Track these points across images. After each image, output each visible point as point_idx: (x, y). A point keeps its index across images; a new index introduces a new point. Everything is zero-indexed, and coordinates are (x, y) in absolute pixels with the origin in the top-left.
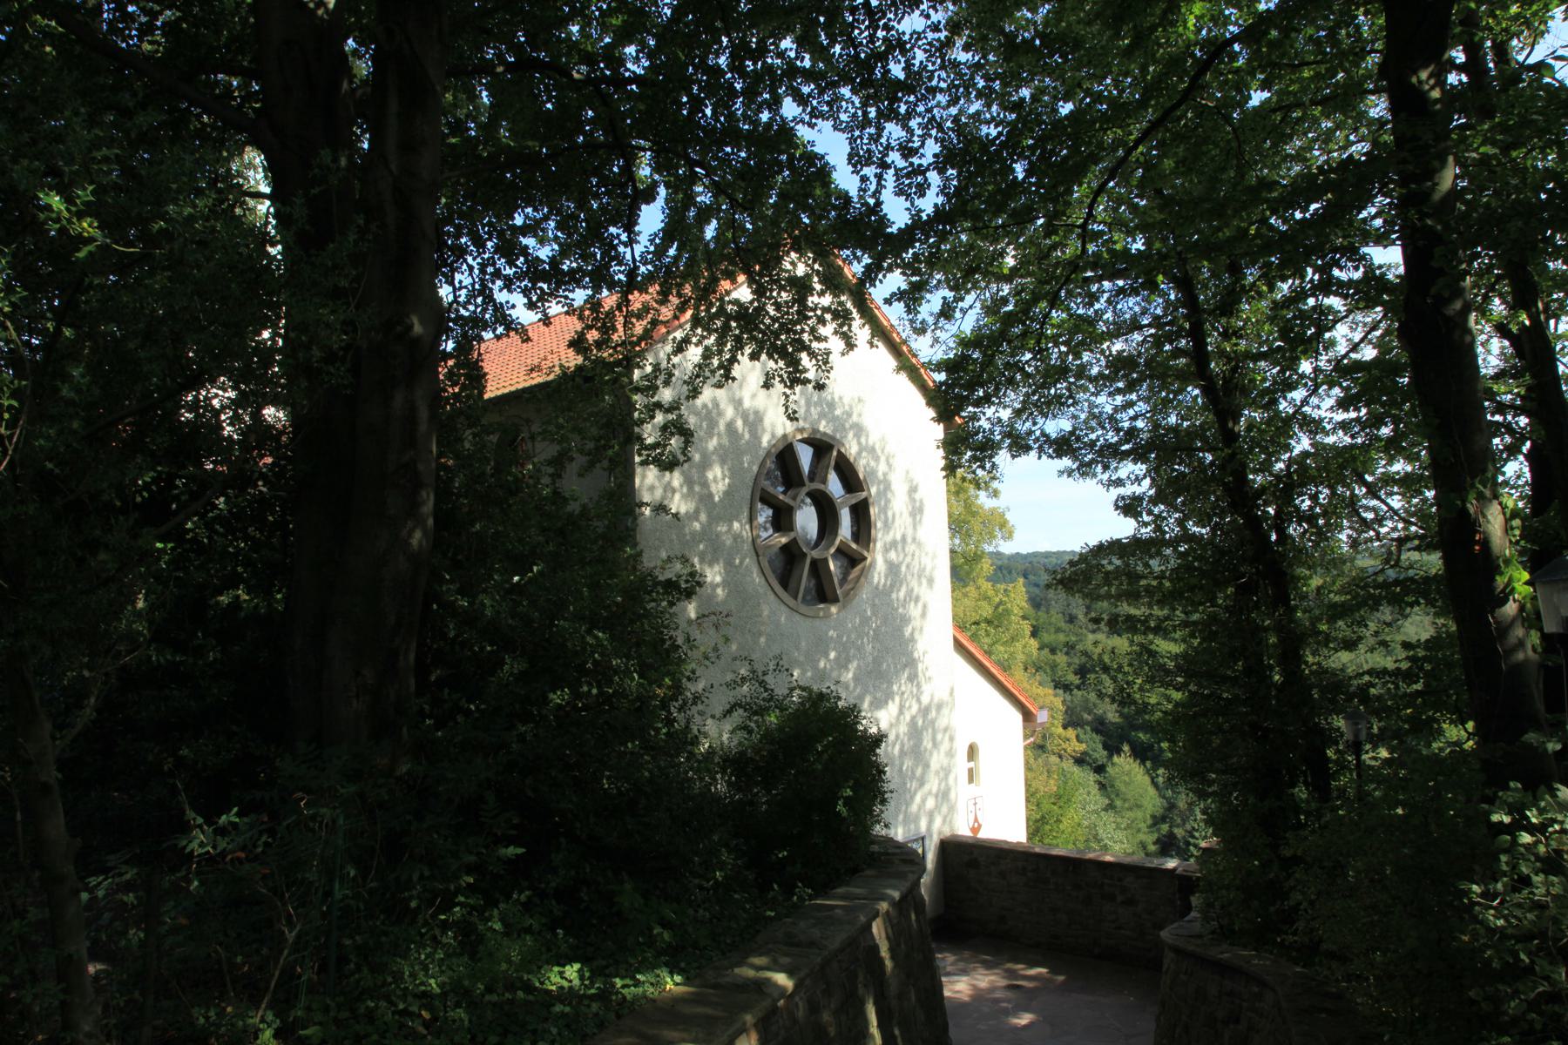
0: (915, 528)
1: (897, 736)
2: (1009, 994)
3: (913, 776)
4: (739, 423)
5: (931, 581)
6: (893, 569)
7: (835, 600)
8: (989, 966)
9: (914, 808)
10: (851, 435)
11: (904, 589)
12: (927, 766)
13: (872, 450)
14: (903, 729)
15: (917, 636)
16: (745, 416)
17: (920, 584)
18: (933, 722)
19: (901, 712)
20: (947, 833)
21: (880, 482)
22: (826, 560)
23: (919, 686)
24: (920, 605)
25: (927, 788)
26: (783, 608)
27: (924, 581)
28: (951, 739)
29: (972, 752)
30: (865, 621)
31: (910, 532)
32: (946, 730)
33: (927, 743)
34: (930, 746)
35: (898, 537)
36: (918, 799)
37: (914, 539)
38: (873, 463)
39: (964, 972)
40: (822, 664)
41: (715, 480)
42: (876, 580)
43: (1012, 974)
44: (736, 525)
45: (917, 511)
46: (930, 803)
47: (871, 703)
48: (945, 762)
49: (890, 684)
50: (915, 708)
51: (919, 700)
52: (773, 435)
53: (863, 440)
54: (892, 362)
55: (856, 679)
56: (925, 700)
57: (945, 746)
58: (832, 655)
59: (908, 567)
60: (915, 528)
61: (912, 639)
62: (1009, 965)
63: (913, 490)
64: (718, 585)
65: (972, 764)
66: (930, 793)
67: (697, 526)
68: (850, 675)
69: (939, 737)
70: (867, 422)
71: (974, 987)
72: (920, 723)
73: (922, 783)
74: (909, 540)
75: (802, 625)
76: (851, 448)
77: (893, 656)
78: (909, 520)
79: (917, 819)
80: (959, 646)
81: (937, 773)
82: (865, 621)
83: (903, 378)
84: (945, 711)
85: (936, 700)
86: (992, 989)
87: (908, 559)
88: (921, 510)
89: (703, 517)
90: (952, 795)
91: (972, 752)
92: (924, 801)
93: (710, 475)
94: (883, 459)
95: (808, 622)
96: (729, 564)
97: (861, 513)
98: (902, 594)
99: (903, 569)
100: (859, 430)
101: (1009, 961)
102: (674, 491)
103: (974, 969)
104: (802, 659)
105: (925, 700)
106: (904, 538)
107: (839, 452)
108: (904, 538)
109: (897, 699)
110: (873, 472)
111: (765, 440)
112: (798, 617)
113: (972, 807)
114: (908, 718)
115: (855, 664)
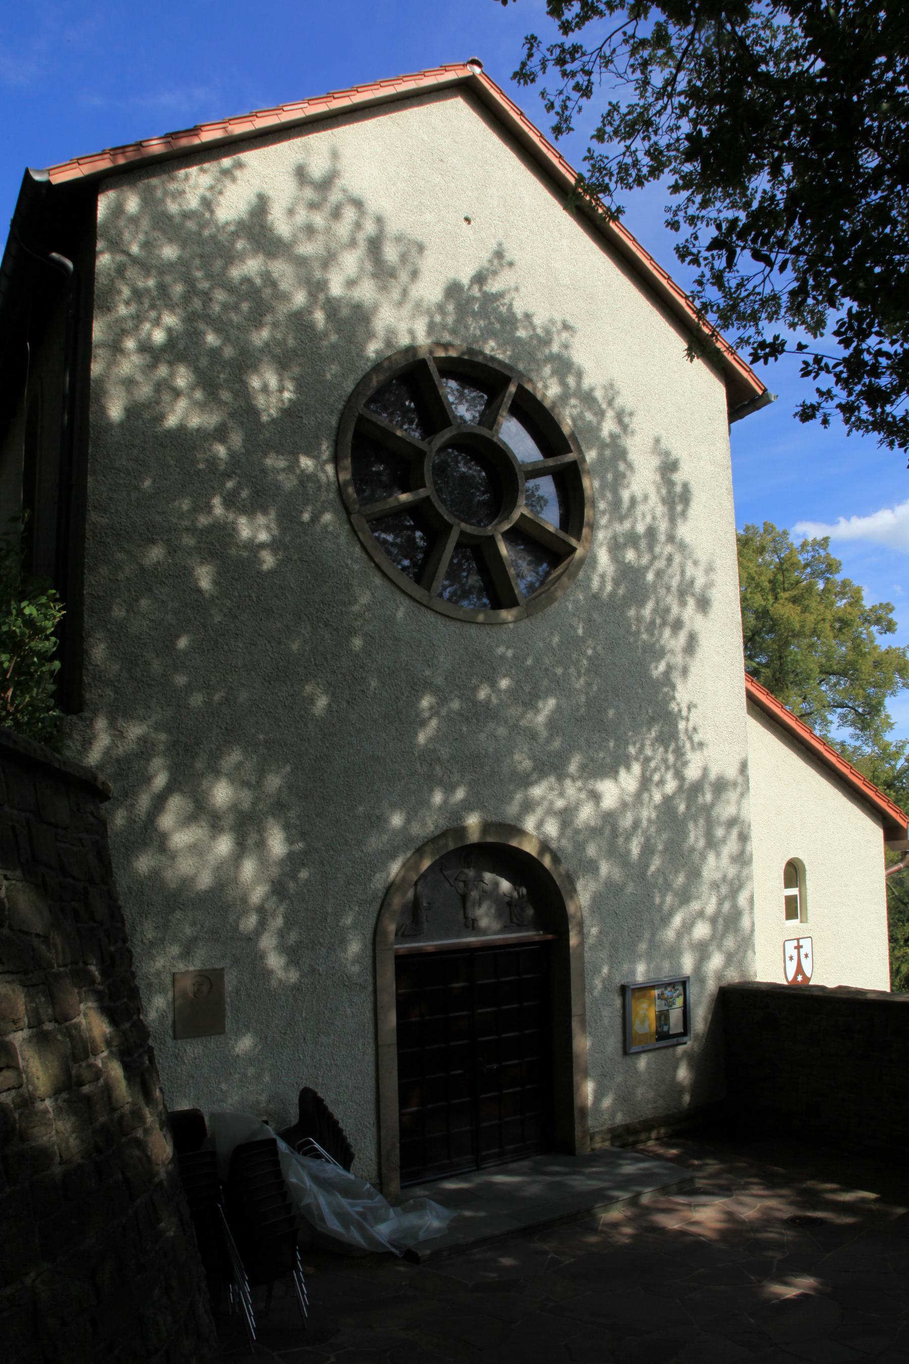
0: (672, 520)
1: (636, 824)
2: (789, 1235)
3: (667, 886)
4: (319, 316)
5: (704, 604)
6: (629, 575)
7: (512, 603)
8: (771, 1182)
9: (670, 934)
10: (547, 370)
11: (650, 605)
12: (695, 874)
13: (588, 399)
14: (647, 813)
15: (676, 677)
16: (332, 308)
17: (683, 604)
18: (707, 810)
19: (645, 783)
20: (733, 977)
21: (603, 446)
22: (492, 540)
23: (679, 753)
24: (682, 637)
25: (695, 906)
26: (399, 597)
27: (691, 602)
28: (744, 838)
29: (794, 872)
30: (572, 643)
31: (663, 526)
32: (732, 822)
33: (695, 836)
34: (701, 843)
35: (641, 528)
36: (677, 920)
37: (671, 538)
38: (589, 416)
39: (724, 1190)
40: (482, 694)
41: (265, 389)
42: (595, 583)
43: (812, 1199)
44: (306, 463)
45: (677, 500)
46: (701, 930)
47: (583, 767)
48: (732, 872)
49: (623, 742)
50: (671, 786)
51: (679, 776)
52: (389, 343)
53: (571, 381)
54: (678, 344)
55: (552, 724)
56: (692, 773)
57: (731, 847)
58: (504, 683)
59: (659, 574)
60: (672, 520)
61: (667, 680)
62: (809, 1184)
63: (669, 467)
64: (263, 546)
65: (794, 891)
66: (701, 914)
67: (221, 450)
68: (541, 719)
69: (720, 832)
70: (579, 356)
71: (730, 1217)
72: (682, 808)
73: (685, 897)
74: (662, 538)
75: (442, 632)
76: (549, 390)
77: (628, 704)
78: (660, 509)
79: (674, 953)
80: (756, 707)
81: (715, 885)
82: (572, 643)
83: (699, 364)
84: (732, 795)
85: (713, 776)
86: (767, 1221)
87: (661, 564)
88: (685, 497)
89: (236, 439)
90: (745, 922)
91: (794, 872)
92: (688, 927)
93: (255, 383)
94: (610, 414)
95: (453, 627)
96: (288, 520)
97: (569, 483)
98: (647, 611)
99: (650, 577)
100: (564, 366)
101: (812, 1178)
102: (177, 394)
103: (746, 1186)
104: (439, 680)
105: (692, 773)
106: (651, 532)
107: (521, 388)
108: (651, 532)
109: (636, 768)
110: (593, 431)
111: (373, 349)
112: (430, 617)
113: (791, 951)
114: (657, 798)
115: (551, 703)
